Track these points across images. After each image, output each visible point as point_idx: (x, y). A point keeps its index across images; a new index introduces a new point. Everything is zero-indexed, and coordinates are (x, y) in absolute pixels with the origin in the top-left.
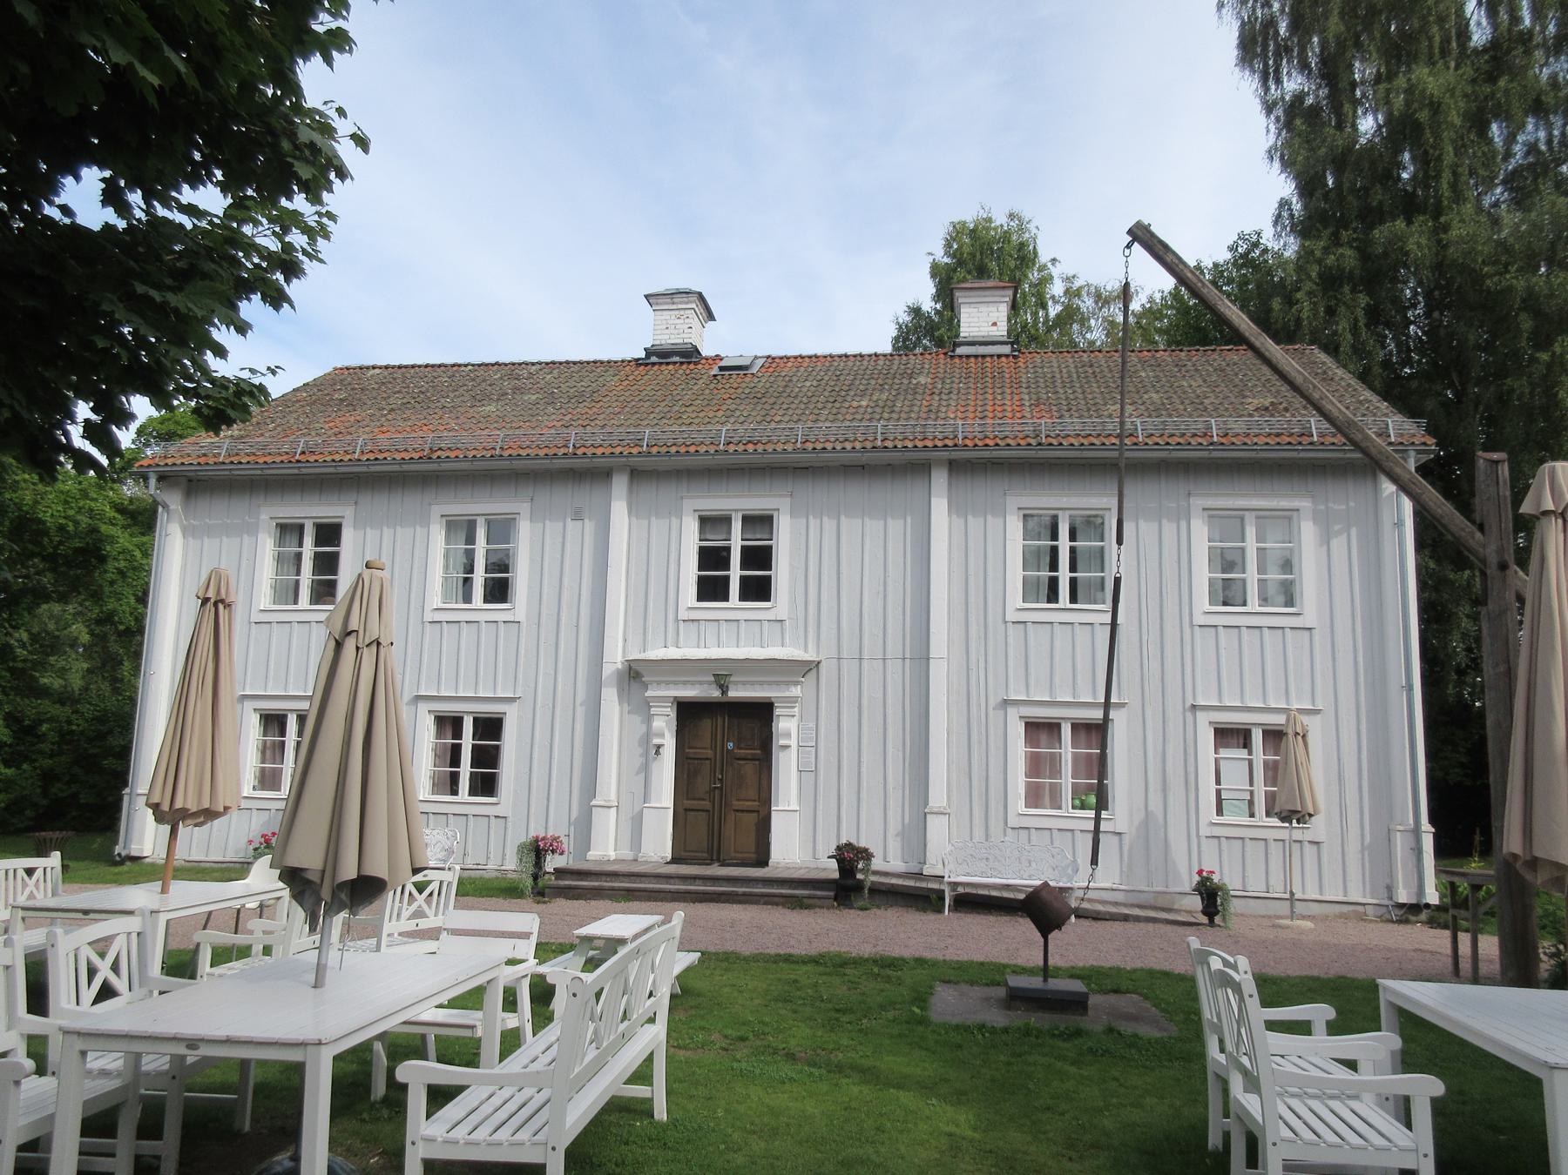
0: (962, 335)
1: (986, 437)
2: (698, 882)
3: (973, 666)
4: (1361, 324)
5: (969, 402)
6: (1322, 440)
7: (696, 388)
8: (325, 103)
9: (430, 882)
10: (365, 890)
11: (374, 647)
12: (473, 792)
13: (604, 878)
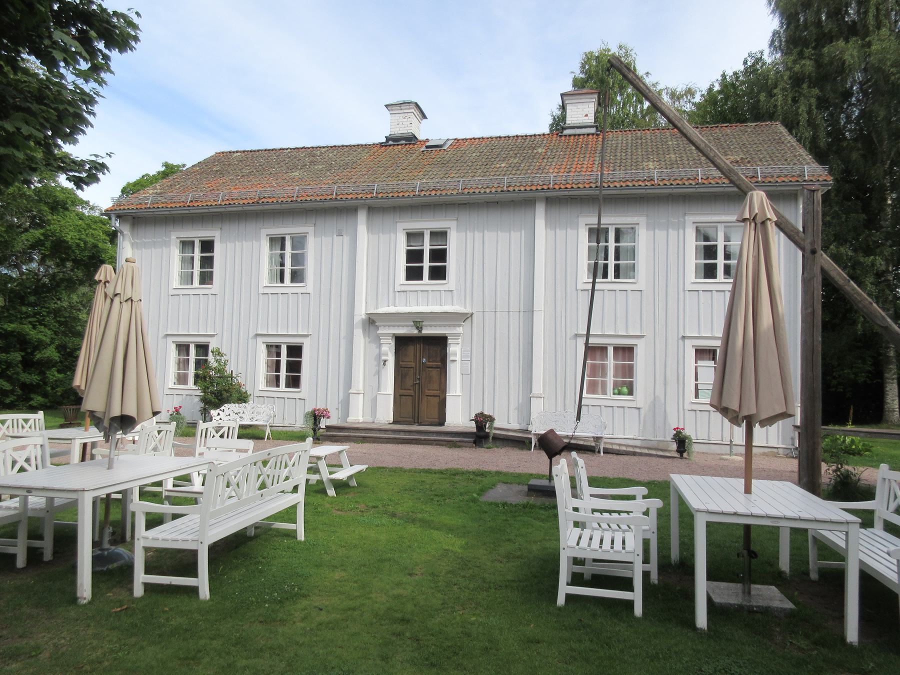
0: (567, 123)
1: (568, 183)
4: (814, 107)
5: (563, 163)
6: (763, 180)
7: (411, 159)
8: (129, 10)
9: (222, 427)
10: (126, 422)
11: (130, 302)
12: (287, 386)
13: (352, 431)
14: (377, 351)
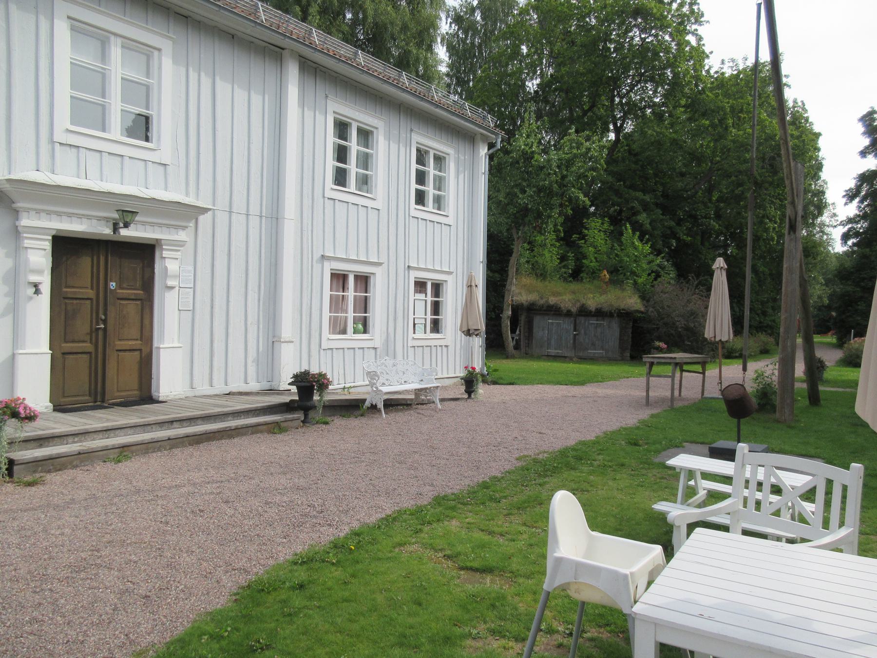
2: (175, 425)
3: (305, 228)
14: (9, 263)
